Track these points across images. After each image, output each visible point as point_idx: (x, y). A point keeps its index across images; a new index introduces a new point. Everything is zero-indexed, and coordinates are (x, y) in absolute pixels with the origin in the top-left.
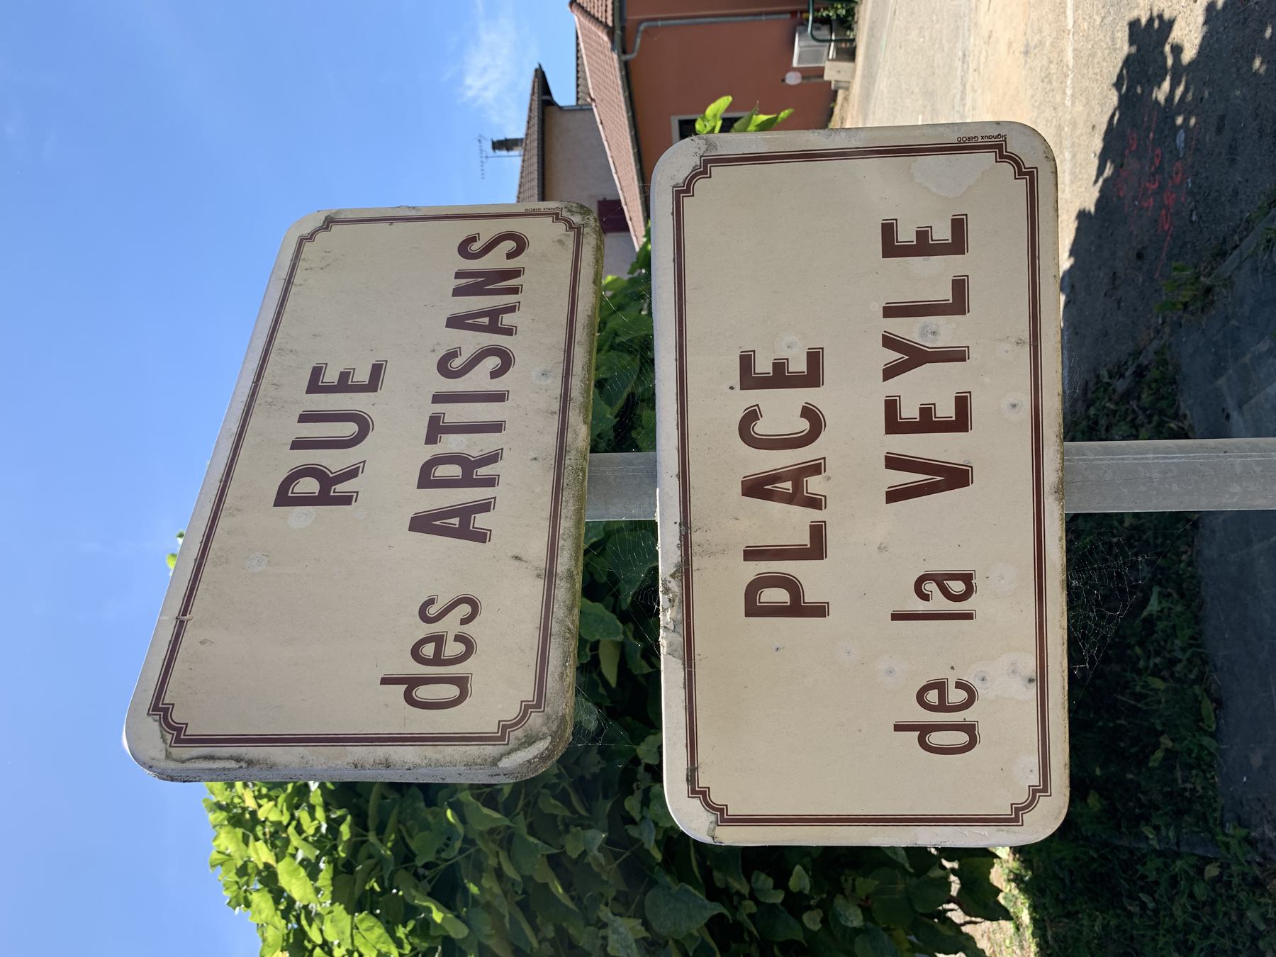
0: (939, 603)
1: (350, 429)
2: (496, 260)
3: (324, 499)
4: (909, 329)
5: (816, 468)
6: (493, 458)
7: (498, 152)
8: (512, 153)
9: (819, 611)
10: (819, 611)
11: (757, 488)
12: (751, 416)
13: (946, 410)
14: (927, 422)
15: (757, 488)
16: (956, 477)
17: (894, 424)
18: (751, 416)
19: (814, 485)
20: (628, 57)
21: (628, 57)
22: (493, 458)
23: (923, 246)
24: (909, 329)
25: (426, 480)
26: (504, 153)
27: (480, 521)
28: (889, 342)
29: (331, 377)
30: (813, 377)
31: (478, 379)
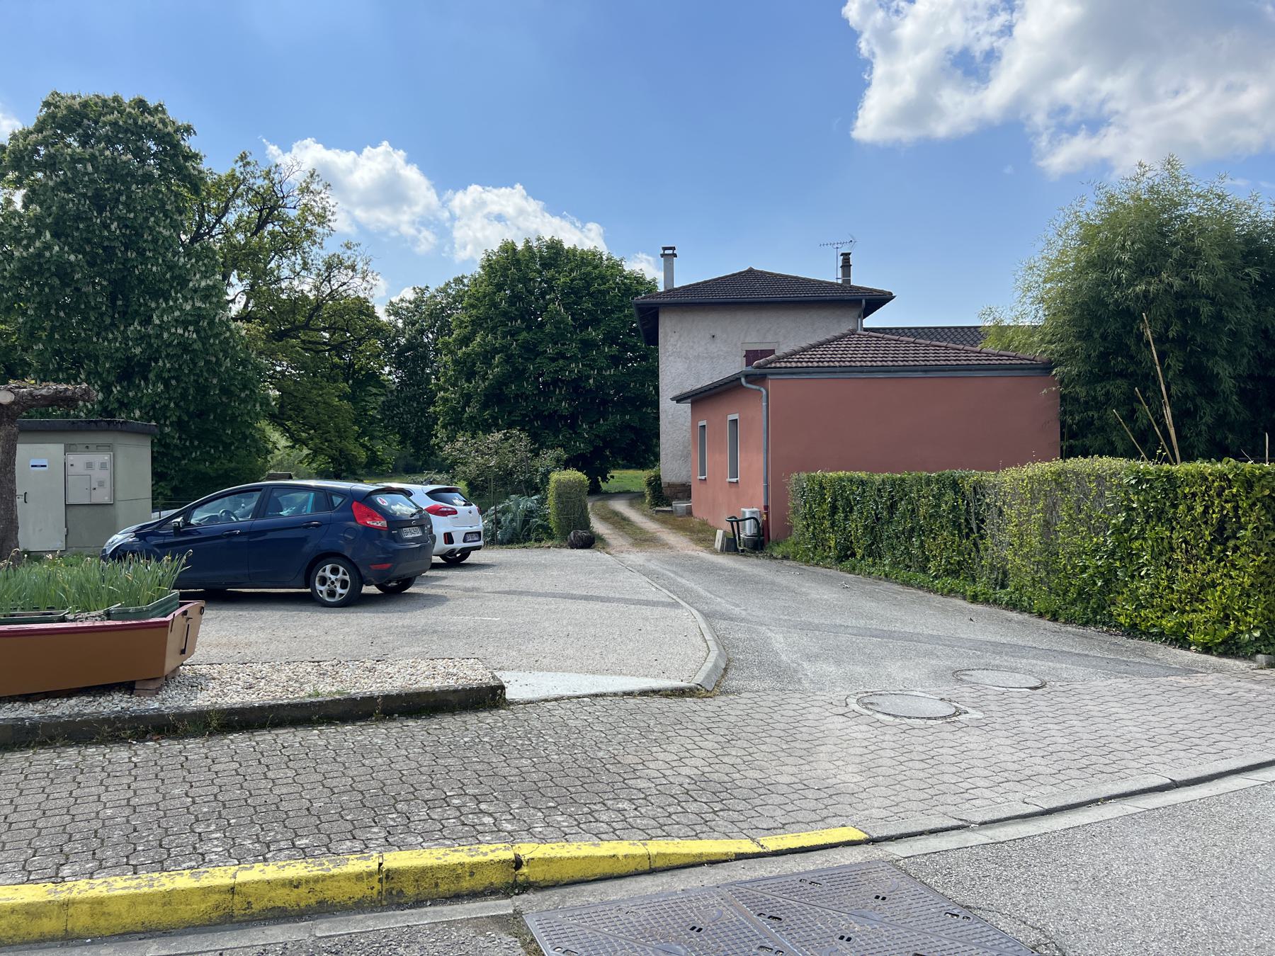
20: (743, 380)
26: (840, 264)
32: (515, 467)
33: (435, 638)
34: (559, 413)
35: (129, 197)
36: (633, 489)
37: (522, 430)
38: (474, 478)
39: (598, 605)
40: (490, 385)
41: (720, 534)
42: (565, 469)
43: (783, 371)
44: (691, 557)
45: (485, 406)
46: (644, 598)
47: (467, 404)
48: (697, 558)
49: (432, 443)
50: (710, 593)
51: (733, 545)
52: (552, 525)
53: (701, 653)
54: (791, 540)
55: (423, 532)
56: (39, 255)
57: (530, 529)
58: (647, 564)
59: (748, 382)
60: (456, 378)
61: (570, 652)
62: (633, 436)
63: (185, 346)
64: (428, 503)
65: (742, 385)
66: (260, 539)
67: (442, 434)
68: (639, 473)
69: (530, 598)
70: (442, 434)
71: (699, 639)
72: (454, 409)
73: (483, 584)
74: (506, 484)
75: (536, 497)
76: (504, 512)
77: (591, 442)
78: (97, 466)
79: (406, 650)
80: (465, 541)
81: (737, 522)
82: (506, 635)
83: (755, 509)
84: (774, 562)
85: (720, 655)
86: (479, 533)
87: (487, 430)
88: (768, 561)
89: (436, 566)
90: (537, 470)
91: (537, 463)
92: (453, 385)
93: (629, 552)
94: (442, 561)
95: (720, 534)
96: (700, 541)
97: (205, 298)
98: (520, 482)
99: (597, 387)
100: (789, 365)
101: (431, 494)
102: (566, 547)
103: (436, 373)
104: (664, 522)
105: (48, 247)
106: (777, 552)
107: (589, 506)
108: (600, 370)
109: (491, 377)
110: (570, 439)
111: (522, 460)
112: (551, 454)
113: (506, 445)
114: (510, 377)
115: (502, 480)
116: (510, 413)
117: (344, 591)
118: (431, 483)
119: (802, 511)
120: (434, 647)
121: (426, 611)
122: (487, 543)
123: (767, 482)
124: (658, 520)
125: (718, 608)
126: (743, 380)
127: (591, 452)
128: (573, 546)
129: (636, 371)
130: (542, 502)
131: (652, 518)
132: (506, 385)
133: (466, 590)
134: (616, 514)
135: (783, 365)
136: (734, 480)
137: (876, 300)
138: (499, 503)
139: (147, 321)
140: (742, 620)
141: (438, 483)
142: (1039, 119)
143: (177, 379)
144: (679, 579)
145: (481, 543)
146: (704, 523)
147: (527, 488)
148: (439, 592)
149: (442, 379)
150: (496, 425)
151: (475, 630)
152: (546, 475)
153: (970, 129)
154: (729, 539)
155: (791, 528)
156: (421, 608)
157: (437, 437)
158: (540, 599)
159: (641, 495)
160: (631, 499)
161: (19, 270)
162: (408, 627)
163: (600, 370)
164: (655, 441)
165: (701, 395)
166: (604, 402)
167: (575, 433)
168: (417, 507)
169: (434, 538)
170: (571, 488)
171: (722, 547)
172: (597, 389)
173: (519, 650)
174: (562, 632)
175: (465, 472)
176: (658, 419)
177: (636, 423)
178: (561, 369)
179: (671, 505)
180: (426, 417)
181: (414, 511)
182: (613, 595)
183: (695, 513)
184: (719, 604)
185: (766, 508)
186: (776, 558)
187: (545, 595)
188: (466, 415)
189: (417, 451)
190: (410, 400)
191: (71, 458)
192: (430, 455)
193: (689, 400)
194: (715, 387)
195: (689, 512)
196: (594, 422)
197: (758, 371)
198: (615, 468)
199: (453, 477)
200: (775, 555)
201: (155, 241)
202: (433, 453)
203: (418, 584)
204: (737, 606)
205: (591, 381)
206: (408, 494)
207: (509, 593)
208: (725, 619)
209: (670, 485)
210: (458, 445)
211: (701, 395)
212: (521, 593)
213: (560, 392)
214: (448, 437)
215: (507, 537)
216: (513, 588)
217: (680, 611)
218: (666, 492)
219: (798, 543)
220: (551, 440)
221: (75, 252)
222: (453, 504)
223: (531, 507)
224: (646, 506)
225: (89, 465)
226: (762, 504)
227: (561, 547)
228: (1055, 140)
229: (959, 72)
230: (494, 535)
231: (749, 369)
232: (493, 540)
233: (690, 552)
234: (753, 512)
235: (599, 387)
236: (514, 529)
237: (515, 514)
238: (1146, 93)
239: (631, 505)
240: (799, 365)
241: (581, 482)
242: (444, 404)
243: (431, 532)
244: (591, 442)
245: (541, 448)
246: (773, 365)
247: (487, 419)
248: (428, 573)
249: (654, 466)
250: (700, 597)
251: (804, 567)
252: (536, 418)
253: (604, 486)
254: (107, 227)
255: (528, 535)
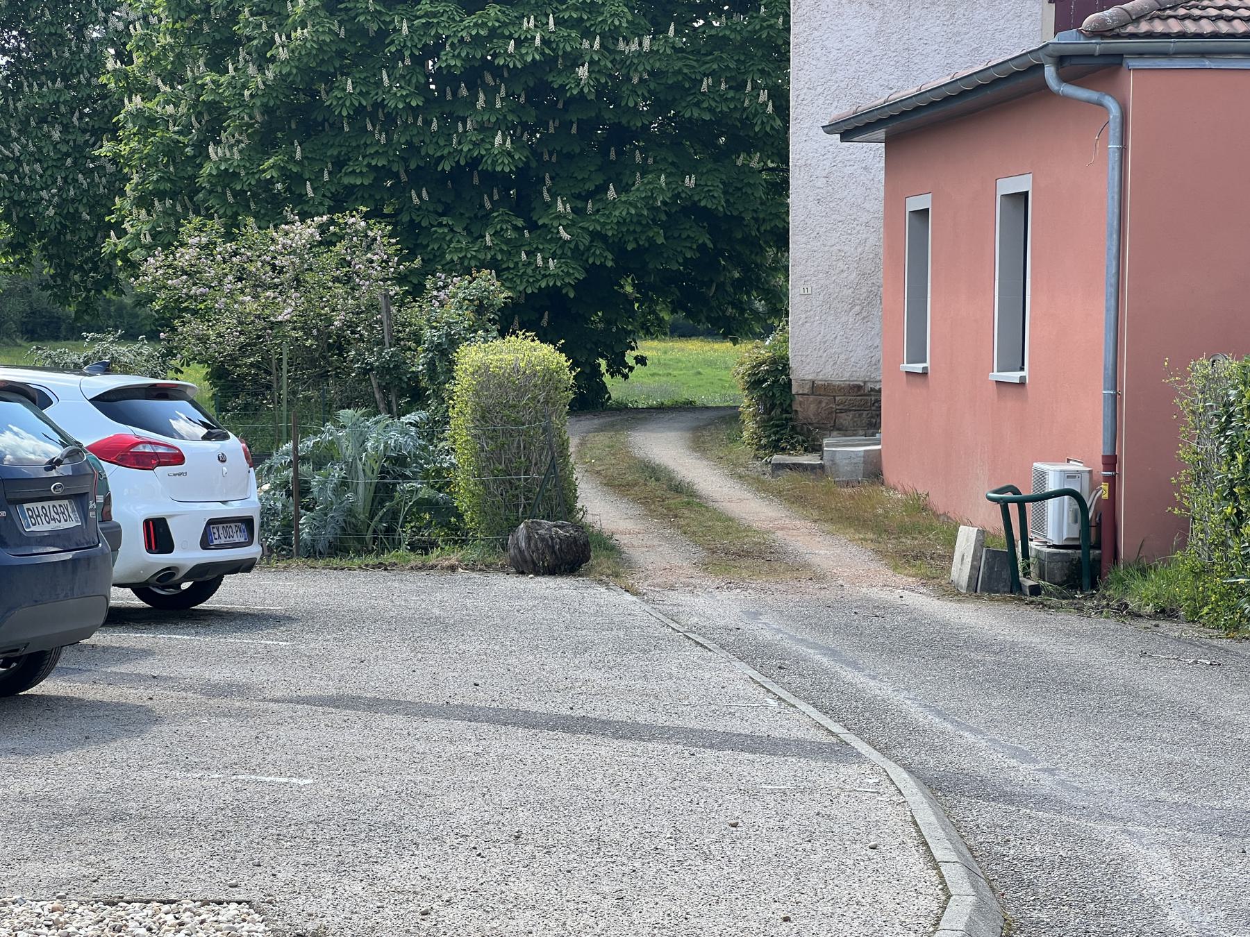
20: (1050, 72)
32: (351, 326)
33: (118, 836)
34: (487, 165)
36: (703, 397)
37: (374, 214)
38: (233, 359)
39: (606, 748)
40: (282, 78)
41: (966, 539)
42: (502, 334)
43: (1171, 44)
44: (880, 609)
45: (264, 142)
46: (736, 726)
47: (212, 133)
48: (900, 609)
49: (106, 249)
50: (939, 713)
51: (1006, 574)
52: (462, 502)
53: (922, 902)
54: (1184, 560)
55: (84, 514)
57: (394, 514)
58: (748, 626)
59: (1064, 78)
60: (179, 56)
61: (524, 887)
62: (705, 239)
64: (105, 429)
65: (1045, 86)
66: (834, 449)
67: (138, 223)
68: (722, 350)
69: (400, 721)
70: (138, 223)
71: (916, 857)
72: (171, 150)
73: (258, 674)
74: (324, 375)
75: (412, 417)
76: (321, 459)
77: (578, 253)
79: (33, 869)
80: (206, 544)
81: (1021, 503)
82: (331, 830)
83: (1074, 467)
84: (1131, 626)
85: (980, 908)
86: (248, 522)
87: (271, 214)
88: (1112, 623)
89: (119, 618)
90: (417, 338)
91: (417, 315)
92: (173, 78)
93: (692, 590)
94: (138, 603)
95: (966, 539)
96: (906, 559)
98: (366, 371)
99: (600, 91)
100: (1191, 27)
101: (107, 402)
102: (502, 569)
103: (119, 40)
104: (796, 500)
106: (1142, 593)
107: (573, 444)
108: (611, 36)
109: (283, 54)
110: (516, 246)
111: (373, 306)
112: (459, 288)
113: (328, 259)
114: (341, 54)
115: (313, 362)
116: (339, 164)
118: (107, 369)
119: (1221, 472)
120: (115, 864)
121: (92, 752)
122: (269, 551)
123: (1114, 382)
124: (779, 494)
125: (967, 764)
126: (1050, 72)
127: (579, 285)
128: (525, 566)
129: (718, 42)
130: (433, 430)
131: (760, 487)
132: (329, 79)
133: (212, 690)
134: (654, 472)
135: (1174, 26)
136: (1014, 376)
138: (305, 433)
140: (1044, 801)
141: (126, 370)
144: (848, 674)
145: (254, 551)
146: (919, 506)
147: (385, 389)
148: (133, 695)
149: (138, 59)
150: (299, 199)
151: (239, 814)
152: (445, 352)
154: (993, 555)
155: (1183, 526)
156: (74, 744)
157: (121, 233)
158: (432, 725)
159: (729, 417)
160: (696, 429)
162: (38, 800)
163: (611, 36)
164: (771, 253)
165: (1003, 89)
166: (621, 135)
167: (533, 226)
168: (65, 440)
169: (115, 535)
170: (521, 390)
171: (973, 578)
172: (599, 94)
173: (373, 879)
174: (500, 826)
175: (203, 340)
176: (781, 187)
177: (716, 202)
178: (493, 33)
179: (816, 448)
180: (88, 173)
181: (57, 451)
182: (650, 717)
183: (890, 475)
184: (971, 748)
185: (1111, 462)
186: (1137, 615)
187: (446, 712)
188: (207, 169)
189: (63, 273)
190: (43, 120)
192: (100, 286)
193: (881, 133)
194: (963, 94)
195: (874, 471)
196: (590, 195)
197: (1097, 46)
198: (649, 334)
199: (170, 353)
200: (1133, 604)
202: (109, 280)
203: (66, 671)
204: (1025, 757)
205: (583, 72)
206: (37, 399)
207: (337, 702)
208: (988, 798)
209: (817, 389)
210: (185, 257)
211: (1003, 89)
212: (374, 705)
213: (490, 103)
214: (155, 235)
215: (328, 534)
216: (350, 689)
217: (853, 770)
218: (806, 409)
219: (1206, 571)
220: (458, 246)
222: (171, 433)
223: (398, 447)
224: (743, 450)
226: (1099, 450)
227: (487, 568)
230: (289, 526)
231: (1070, 39)
232: (286, 541)
233: (877, 594)
234: (1071, 476)
235: (608, 91)
236: (350, 512)
237: (351, 467)
239: (699, 446)
240: (1223, 27)
241: (550, 376)
242: (143, 134)
243: (106, 516)
244: (578, 253)
245: (428, 269)
246: (1144, 27)
247: (271, 181)
248: (101, 638)
249: (770, 330)
250: (910, 728)
251: (1224, 643)
252: (418, 178)
253: (615, 387)
255: (390, 530)
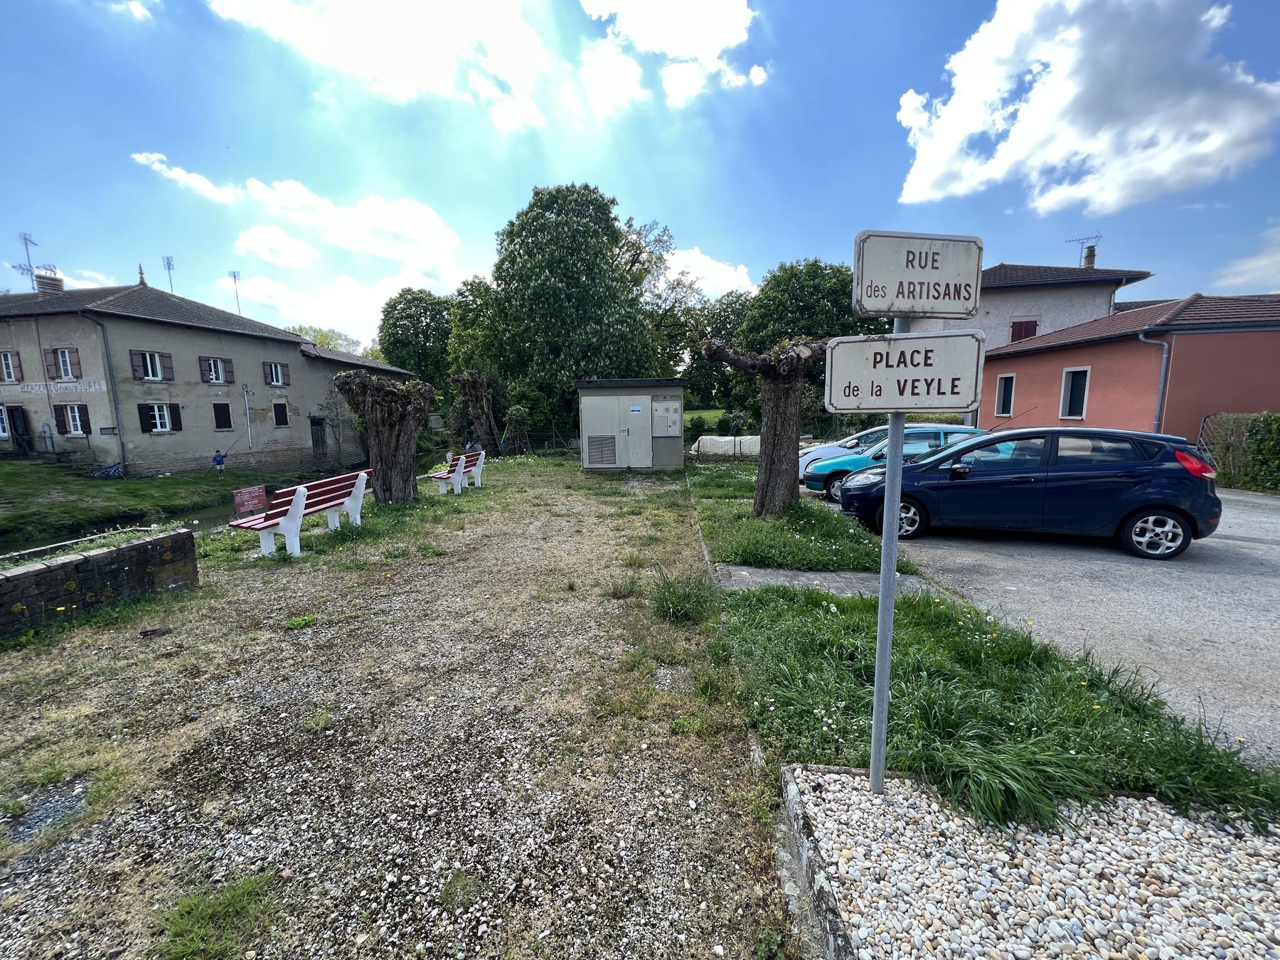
0: (875, 390)
1: (923, 265)
2: (963, 293)
3: (908, 261)
4: (935, 384)
5: (905, 366)
6: (914, 297)
7: (1085, 251)
8: (1083, 260)
9: (875, 367)
10: (875, 367)
11: (903, 353)
12: (918, 352)
13: (916, 391)
14: (914, 387)
15: (903, 353)
16: (901, 393)
17: (914, 381)
18: (918, 352)
19: (902, 365)
20: (1141, 337)
21: (1141, 337)
22: (914, 297)
23: (954, 386)
24: (935, 384)
25: (910, 283)
26: (1084, 255)
27: (901, 296)
28: (933, 380)
29: (936, 257)
30: (926, 364)
31: (933, 292)
35: (586, 246)
56: (543, 284)
63: (623, 336)
78: (671, 411)
97: (631, 306)
105: (547, 279)
117: (913, 510)
123: (1160, 419)
137: (1117, 280)
139: (599, 322)
142: (1034, 176)
143: (616, 356)
153: (982, 188)
161: (533, 294)
191: (656, 405)
201: (600, 272)
221: (561, 281)
225: (667, 410)
228: (1044, 190)
229: (976, 153)
238: (1121, 149)
254: (575, 265)
